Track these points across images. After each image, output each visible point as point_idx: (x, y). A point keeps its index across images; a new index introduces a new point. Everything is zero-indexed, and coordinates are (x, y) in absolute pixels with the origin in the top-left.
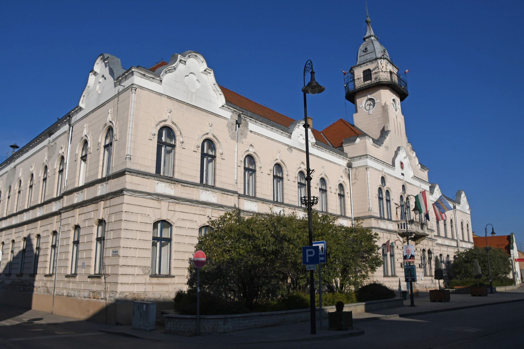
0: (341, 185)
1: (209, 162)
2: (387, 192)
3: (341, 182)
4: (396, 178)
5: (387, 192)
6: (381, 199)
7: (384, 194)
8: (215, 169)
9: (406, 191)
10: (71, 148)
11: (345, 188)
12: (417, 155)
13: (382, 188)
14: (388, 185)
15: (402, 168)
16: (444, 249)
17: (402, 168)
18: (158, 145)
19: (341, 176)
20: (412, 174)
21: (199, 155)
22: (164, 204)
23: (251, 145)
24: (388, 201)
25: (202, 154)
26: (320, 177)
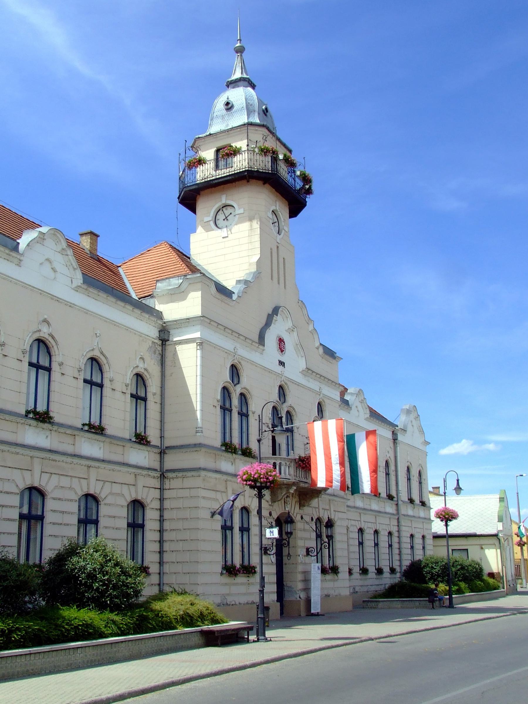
0: (139, 378)
2: (243, 397)
3: (140, 370)
4: (265, 369)
5: (243, 397)
6: (226, 409)
7: (235, 401)
8: (231, 429)
9: (287, 398)
11: (149, 382)
13: (231, 388)
14: (291, 400)
15: (282, 350)
16: (369, 518)
17: (282, 351)
19: (142, 358)
20: (302, 365)
24: (244, 415)
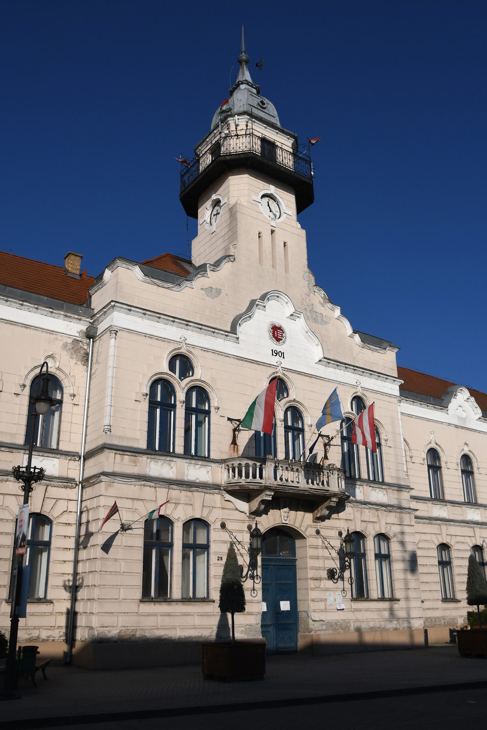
1: (294, 439)
10: (44, 421)
12: (344, 313)
18: (186, 413)
21: (145, 405)
22: (198, 496)
23: (466, 444)
25: (150, 402)
26: (428, 448)
